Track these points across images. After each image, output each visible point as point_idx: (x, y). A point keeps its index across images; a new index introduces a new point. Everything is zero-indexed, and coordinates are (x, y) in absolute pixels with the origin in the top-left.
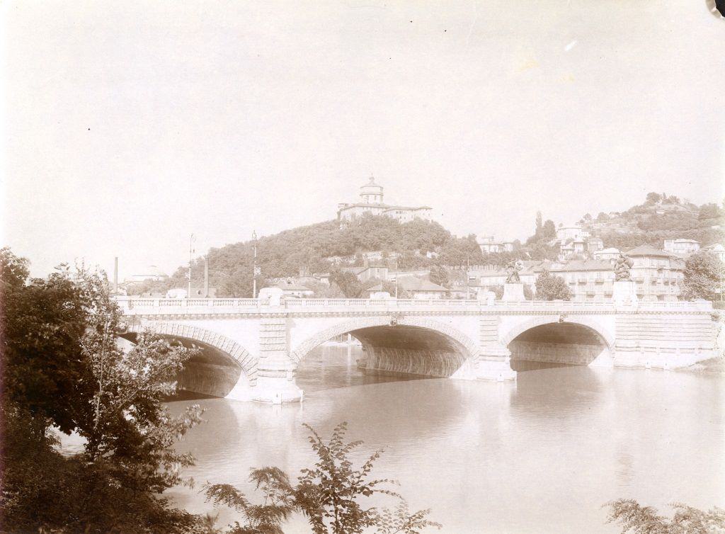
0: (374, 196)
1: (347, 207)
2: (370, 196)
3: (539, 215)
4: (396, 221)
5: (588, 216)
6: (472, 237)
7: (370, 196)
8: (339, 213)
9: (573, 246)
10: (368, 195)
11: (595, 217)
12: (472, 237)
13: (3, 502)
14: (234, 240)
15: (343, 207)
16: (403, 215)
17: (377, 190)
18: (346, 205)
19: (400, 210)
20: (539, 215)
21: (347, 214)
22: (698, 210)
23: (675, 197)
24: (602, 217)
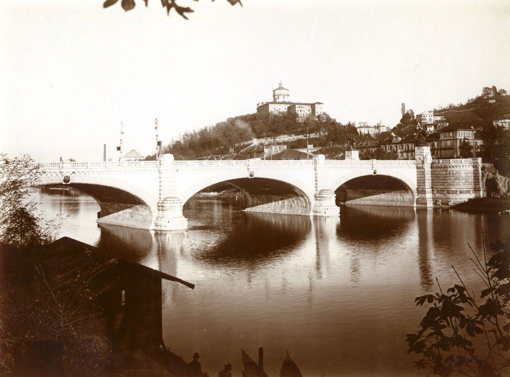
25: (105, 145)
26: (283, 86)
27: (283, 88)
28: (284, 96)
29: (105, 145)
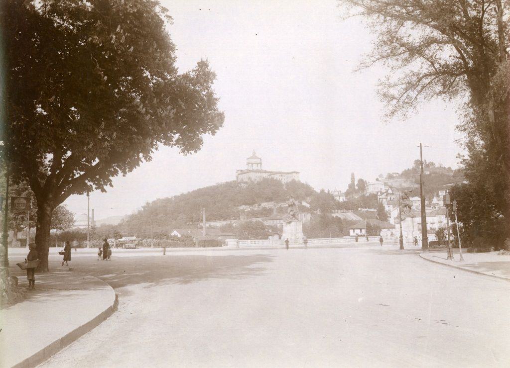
0: (256, 165)
1: (242, 172)
2: (254, 165)
3: (353, 175)
4: (245, 205)
5: (381, 176)
6: (216, 75)
7: (254, 165)
8: (237, 177)
9: (387, 195)
10: (252, 164)
11: (385, 176)
12: (216, 75)
13: (465, 4)
14: (162, 196)
15: (239, 172)
16: (284, 178)
17: (258, 160)
18: (241, 171)
19: (281, 174)
20: (353, 175)
21: (245, 177)
22: (452, 171)
23: (433, 163)
24: (390, 177)
25: (421, 144)
26: (257, 155)
27: (256, 157)
28: (257, 164)
29: (421, 144)
